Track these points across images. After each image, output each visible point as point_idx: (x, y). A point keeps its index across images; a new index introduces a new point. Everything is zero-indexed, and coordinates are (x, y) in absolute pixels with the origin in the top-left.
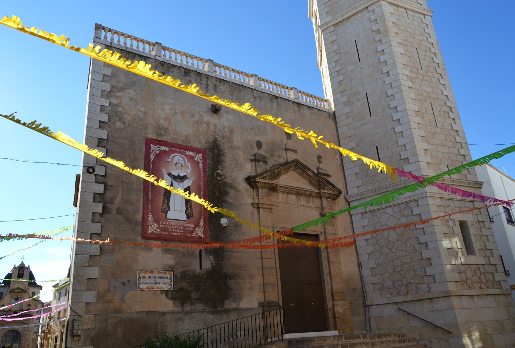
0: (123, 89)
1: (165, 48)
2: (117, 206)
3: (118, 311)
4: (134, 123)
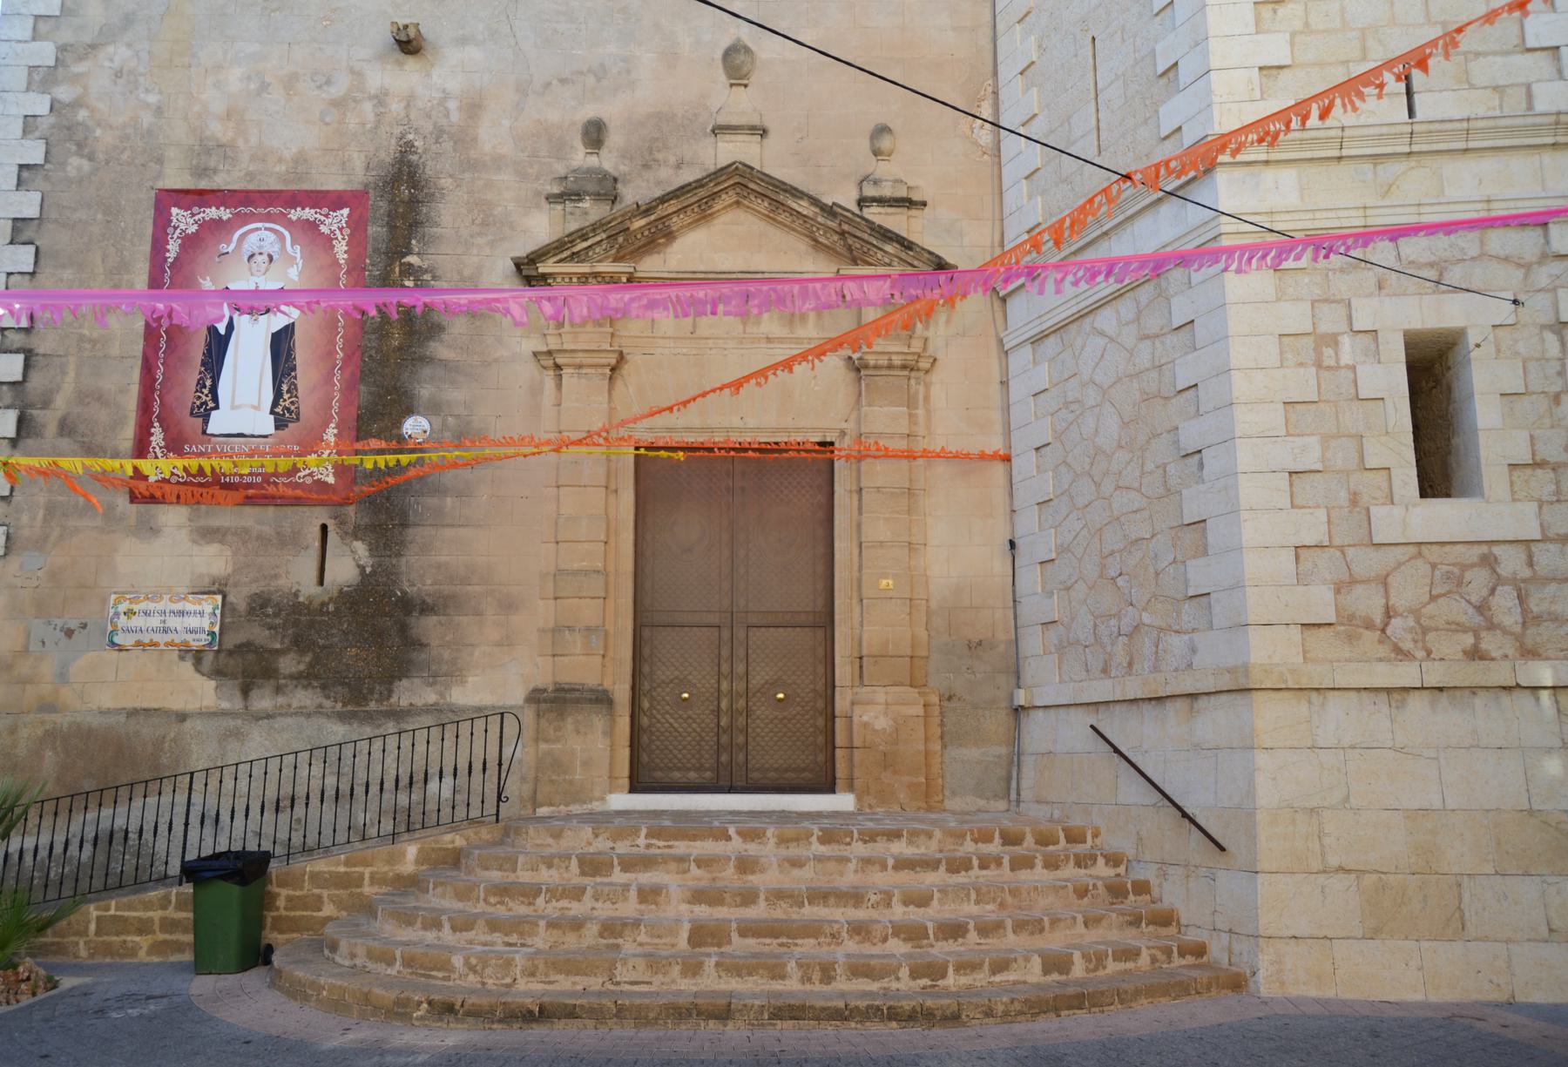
2: (59, 414)
3: (47, 707)
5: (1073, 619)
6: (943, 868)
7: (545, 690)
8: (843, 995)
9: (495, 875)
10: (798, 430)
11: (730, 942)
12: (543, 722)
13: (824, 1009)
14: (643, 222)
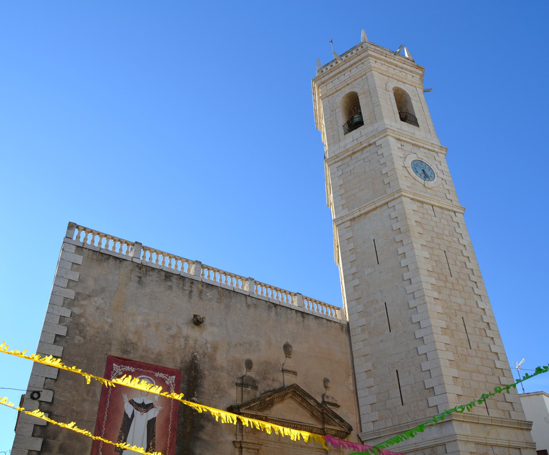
0: (89, 296)
1: (145, 249)
4: (97, 337)
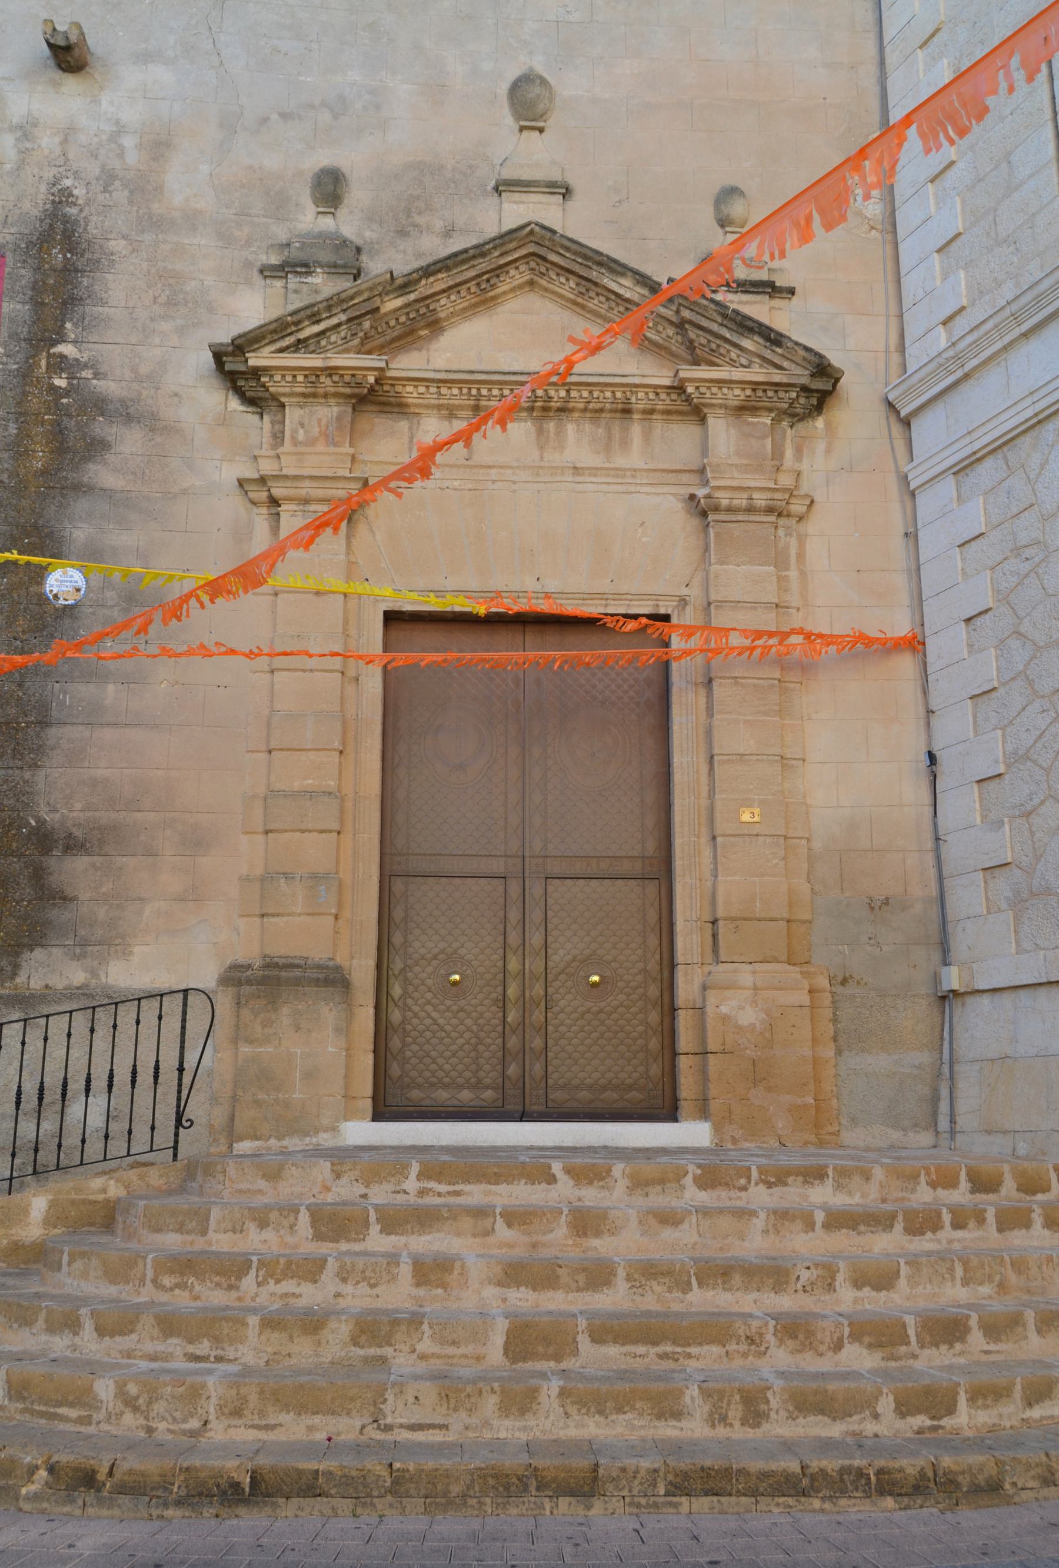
5: (1038, 859)
6: (899, 1227)
7: (249, 967)
8: (787, 1446)
9: (172, 1241)
10: (619, 596)
11: (575, 1352)
12: (246, 1013)
13: (764, 1475)
14: (398, 302)
